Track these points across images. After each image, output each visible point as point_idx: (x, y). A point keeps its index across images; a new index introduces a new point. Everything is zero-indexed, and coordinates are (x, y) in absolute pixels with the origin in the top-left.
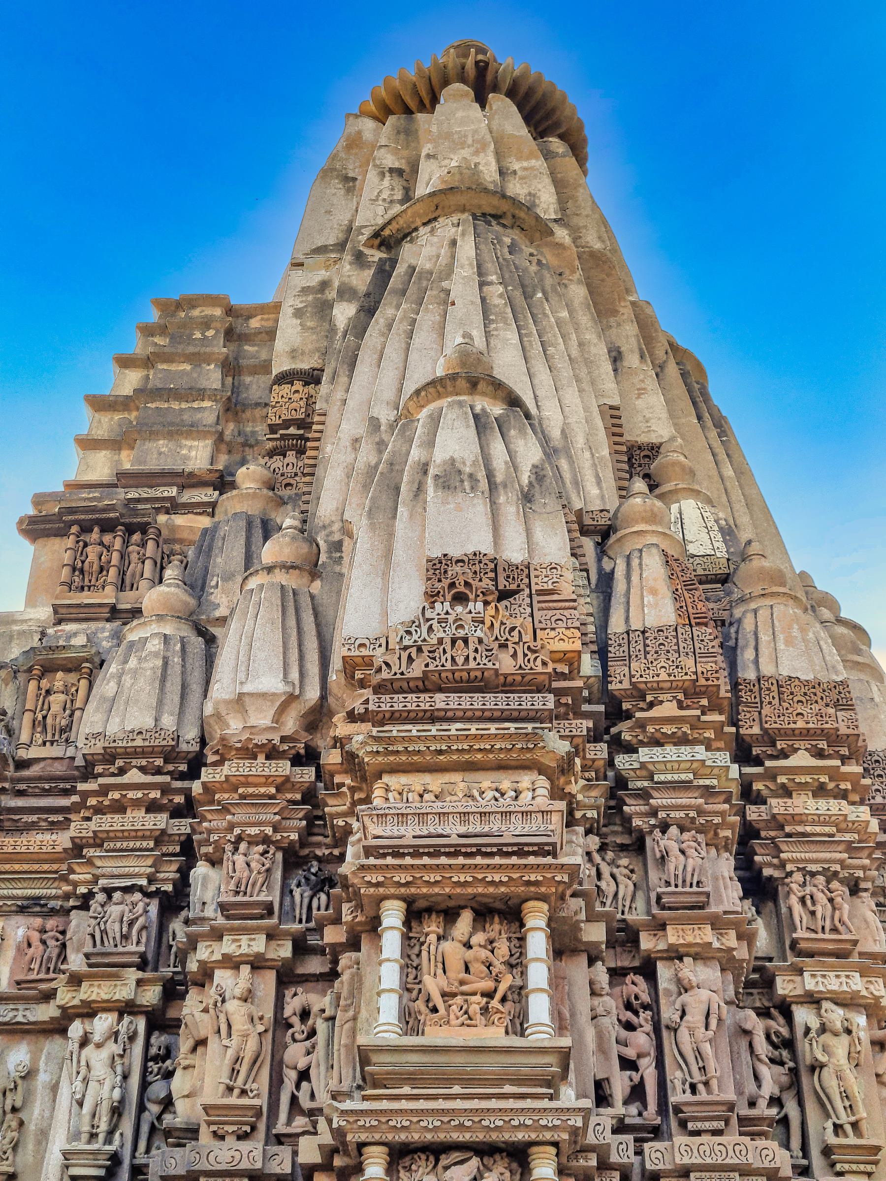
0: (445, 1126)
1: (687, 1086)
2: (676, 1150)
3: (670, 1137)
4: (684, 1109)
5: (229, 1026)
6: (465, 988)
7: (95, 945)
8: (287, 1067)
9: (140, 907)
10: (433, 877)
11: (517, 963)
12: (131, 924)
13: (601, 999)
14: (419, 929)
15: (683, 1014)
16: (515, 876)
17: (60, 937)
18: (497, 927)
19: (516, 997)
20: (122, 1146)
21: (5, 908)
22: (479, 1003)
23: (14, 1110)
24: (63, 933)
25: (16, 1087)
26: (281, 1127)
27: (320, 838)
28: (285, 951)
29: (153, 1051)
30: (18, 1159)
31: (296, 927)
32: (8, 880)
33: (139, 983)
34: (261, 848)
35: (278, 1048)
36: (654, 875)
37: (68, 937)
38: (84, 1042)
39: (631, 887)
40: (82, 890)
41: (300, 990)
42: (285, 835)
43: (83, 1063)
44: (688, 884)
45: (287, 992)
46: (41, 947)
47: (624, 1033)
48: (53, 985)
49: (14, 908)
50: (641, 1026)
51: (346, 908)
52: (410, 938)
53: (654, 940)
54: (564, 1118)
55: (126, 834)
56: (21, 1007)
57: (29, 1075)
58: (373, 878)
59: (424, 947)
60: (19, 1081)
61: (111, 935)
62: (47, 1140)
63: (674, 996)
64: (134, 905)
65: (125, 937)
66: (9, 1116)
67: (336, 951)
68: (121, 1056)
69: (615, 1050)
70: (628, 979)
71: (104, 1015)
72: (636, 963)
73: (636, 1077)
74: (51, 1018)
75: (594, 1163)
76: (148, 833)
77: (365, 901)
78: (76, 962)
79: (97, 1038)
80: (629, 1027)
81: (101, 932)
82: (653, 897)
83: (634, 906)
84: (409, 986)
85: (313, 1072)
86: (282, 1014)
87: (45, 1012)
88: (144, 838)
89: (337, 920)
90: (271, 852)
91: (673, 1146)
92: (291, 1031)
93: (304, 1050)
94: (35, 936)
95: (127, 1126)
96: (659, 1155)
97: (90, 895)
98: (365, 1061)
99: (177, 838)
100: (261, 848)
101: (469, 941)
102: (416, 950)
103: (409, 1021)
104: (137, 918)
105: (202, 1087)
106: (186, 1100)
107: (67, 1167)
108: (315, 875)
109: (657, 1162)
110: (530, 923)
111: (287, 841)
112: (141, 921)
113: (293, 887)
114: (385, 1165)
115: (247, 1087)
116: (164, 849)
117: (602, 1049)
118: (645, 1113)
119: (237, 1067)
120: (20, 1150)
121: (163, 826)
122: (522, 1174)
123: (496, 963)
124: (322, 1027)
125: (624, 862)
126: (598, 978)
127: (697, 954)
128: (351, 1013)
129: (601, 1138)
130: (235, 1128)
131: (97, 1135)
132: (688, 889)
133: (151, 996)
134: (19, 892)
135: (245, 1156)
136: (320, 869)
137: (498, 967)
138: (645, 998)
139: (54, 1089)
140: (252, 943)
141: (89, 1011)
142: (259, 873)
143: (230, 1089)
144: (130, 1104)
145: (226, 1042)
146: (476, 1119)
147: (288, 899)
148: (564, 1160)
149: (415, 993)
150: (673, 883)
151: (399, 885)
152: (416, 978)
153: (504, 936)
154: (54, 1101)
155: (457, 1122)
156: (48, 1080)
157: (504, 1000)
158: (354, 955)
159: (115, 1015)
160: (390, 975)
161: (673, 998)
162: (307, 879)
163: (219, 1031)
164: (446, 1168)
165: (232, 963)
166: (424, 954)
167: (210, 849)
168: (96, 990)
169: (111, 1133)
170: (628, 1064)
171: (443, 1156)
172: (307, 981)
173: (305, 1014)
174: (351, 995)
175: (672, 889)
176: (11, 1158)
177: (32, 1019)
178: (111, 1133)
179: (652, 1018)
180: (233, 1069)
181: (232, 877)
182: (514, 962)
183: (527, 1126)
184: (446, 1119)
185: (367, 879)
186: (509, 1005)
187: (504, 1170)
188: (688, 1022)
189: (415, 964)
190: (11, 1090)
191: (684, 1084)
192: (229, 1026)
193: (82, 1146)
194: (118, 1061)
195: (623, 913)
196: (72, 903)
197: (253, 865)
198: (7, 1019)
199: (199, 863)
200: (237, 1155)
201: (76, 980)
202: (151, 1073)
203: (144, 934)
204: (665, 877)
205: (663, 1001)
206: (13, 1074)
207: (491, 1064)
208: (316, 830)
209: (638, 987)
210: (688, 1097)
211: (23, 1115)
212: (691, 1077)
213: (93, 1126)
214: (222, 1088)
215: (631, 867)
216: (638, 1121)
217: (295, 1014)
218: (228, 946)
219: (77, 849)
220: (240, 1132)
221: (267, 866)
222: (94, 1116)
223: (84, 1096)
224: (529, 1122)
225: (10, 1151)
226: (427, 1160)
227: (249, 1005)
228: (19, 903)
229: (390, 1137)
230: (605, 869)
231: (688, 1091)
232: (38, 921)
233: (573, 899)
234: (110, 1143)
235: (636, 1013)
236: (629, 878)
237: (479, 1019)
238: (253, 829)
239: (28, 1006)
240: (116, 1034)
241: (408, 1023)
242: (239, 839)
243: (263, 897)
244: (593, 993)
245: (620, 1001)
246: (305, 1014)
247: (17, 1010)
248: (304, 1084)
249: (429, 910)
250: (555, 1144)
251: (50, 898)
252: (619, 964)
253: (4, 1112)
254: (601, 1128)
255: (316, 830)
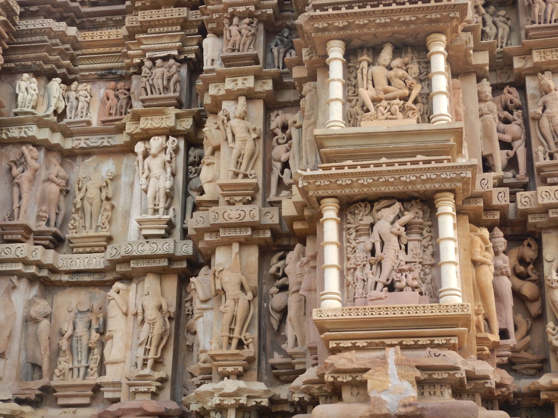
0: (375, 183)
1: (547, 155)
2: (539, 195)
3: (535, 189)
4: (545, 169)
5: (234, 135)
6: (389, 95)
7: (147, 94)
8: (275, 160)
9: (174, 69)
10: (362, 21)
11: (425, 77)
12: (169, 80)
13: (486, 104)
14: (355, 61)
15: (544, 108)
16: (420, 16)
17: (127, 92)
18: (410, 55)
19: (425, 100)
20: (175, 217)
21: (91, 77)
22: (398, 104)
23: (108, 199)
24: (129, 90)
25: (107, 185)
26: (272, 197)
27: (289, 13)
28: (269, 86)
29: (191, 159)
30: (112, 228)
31: (274, 70)
32: (90, 58)
33: (178, 116)
34: (247, 20)
35: (267, 149)
36: (524, 21)
37: (131, 91)
38: (146, 155)
39: (507, 28)
40: (137, 61)
41: (280, 112)
42: (264, 11)
43: (146, 167)
44: (548, 21)
45: (272, 114)
46: (116, 100)
47: (502, 126)
48: (123, 121)
49: (96, 76)
50: (515, 120)
51: (304, 51)
52: (349, 67)
53: (524, 61)
54: (458, 172)
55: (161, 22)
56: (106, 137)
57: (114, 178)
58: (321, 25)
59: (359, 71)
60: (109, 182)
61: (156, 87)
62: (129, 216)
63: (538, 98)
64: (170, 67)
65: (166, 89)
66: (105, 202)
67: (302, 81)
68: (170, 162)
69: (496, 136)
70: (505, 90)
71: (156, 137)
72: (511, 80)
73: (511, 153)
74: (125, 142)
75: (481, 204)
76: (176, 21)
77: (317, 42)
78: (137, 106)
79: (153, 151)
80: (506, 121)
81: (150, 85)
82: (523, 33)
83: (509, 42)
84: (350, 98)
85: (291, 163)
86: (270, 127)
87: (120, 140)
88: (173, 24)
89: (300, 63)
90: (255, 22)
91: (536, 193)
92: (276, 138)
93: (284, 149)
94: (111, 93)
95: (177, 205)
96: (527, 199)
97: (142, 63)
98: (320, 146)
99: (195, 23)
100: (247, 20)
101: (390, 64)
102: (354, 75)
103: (350, 119)
104: (172, 76)
105: (219, 176)
106: (210, 184)
107: (141, 230)
108: (287, 38)
109: (525, 204)
110: (433, 48)
111: (265, 15)
112: (175, 76)
113: (273, 47)
114: (337, 211)
115: (248, 173)
116: (188, 32)
117: (487, 135)
118: (518, 176)
119: (240, 160)
120: (113, 222)
121: (185, 15)
122: (431, 213)
123: (410, 77)
124: (294, 132)
125: (502, 13)
126: (484, 90)
127: (554, 69)
128: (312, 120)
129: (486, 188)
130: (241, 198)
131: (158, 210)
132: (548, 25)
133: (187, 124)
134: (98, 66)
135: (247, 213)
136: (290, 34)
137: (411, 80)
138: (518, 101)
139: (132, 185)
140: (244, 82)
141: (146, 136)
142: (247, 36)
143: (236, 175)
144: (178, 192)
145: (231, 145)
146: (397, 177)
147: (269, 55)
148: (460, 203)
149: (354, 102)
150: (537, 21)
151: (339, 29)
152: (354, 92)
153: (415, 60)
154: (132, 192)
155: (383, 179)
156: (127, 180)
157: (415, 102)
158: (312, 83)
159: (164, 138)
160: (336, 90)
161: (537, 100)
162: (282, 41)
163: (227, 139)
164: (378, 211)
165: (233, 96)
166: (359, 75)
167: (214, 25)
168: (150, 122)
169: (167, 209)
170: (505, 145)
171: (376, 204)
172: (285, 107)
173: (285, 127)
174: (312, 108)
175: (536, 25)
176: (108, 227)
177: (113, 143)
178: (167, 209)
179: (523, 114)
180: (238, 162)
181: (229, 41)
182: (423, 78)
183: (432, 179)
184: (376, 178)
185: (316, 25)
186: (419, 105)
187: (418, 210)
188: (548, 113)
189: (353, 84)
190: (104, 187)
191: (544, 154)
192: (234, 135)
193: (150, 216)
194: (168, 165)
195: (501, 47)
196: (132, 70)
197: (243, 31)
198: (97, 144)
199: (208, 35)
200: (243, 214)
201: (136, 117)
202: (191, 173)
203: (178, 86)
204: (532, 19)
205: (530, 102)
206: (105, 178)
207: (406, 144)
208: (287, 8)
209: (511, 95)
210: (548, 161)
211: (113, 202)
212: (550, 149)
213: (155, 205)
214: (231, 174)
215: (507, 16)
216: (513, 180)
217: (278, 127)
218: (229, 85)
219: (132, 34)
220: (244, 200)
221: (253, 31)
222: (155, 198)
223: (147, 187)
224: (433, 177)
225: (106, 223)
226: (365, 207)
227: (245, 122)
228: (99, 73)
229: (339, 192)
230: (489, 19)
231: (548, 158)
232: (112, 84)
233: (464, 34)
234: (167, 214)
235: (512, 113)
236: (506, 24)
237: (400, 115)
238: (241, 8)
239: (110, 136)
240: (166, 148)
241: (350, 122)
242: (233, 16)
243: (251, 52)
244: (481, 100)
245: (500, 105)
246: (285, 127)
247: (103, 138)
248: (286, 170)
249: (361, 48)
250: (452, 191)
251: (118, 68)
252: (499, 81)
253: (102, 201)
254: (485, 182)
255: (287, 8)
